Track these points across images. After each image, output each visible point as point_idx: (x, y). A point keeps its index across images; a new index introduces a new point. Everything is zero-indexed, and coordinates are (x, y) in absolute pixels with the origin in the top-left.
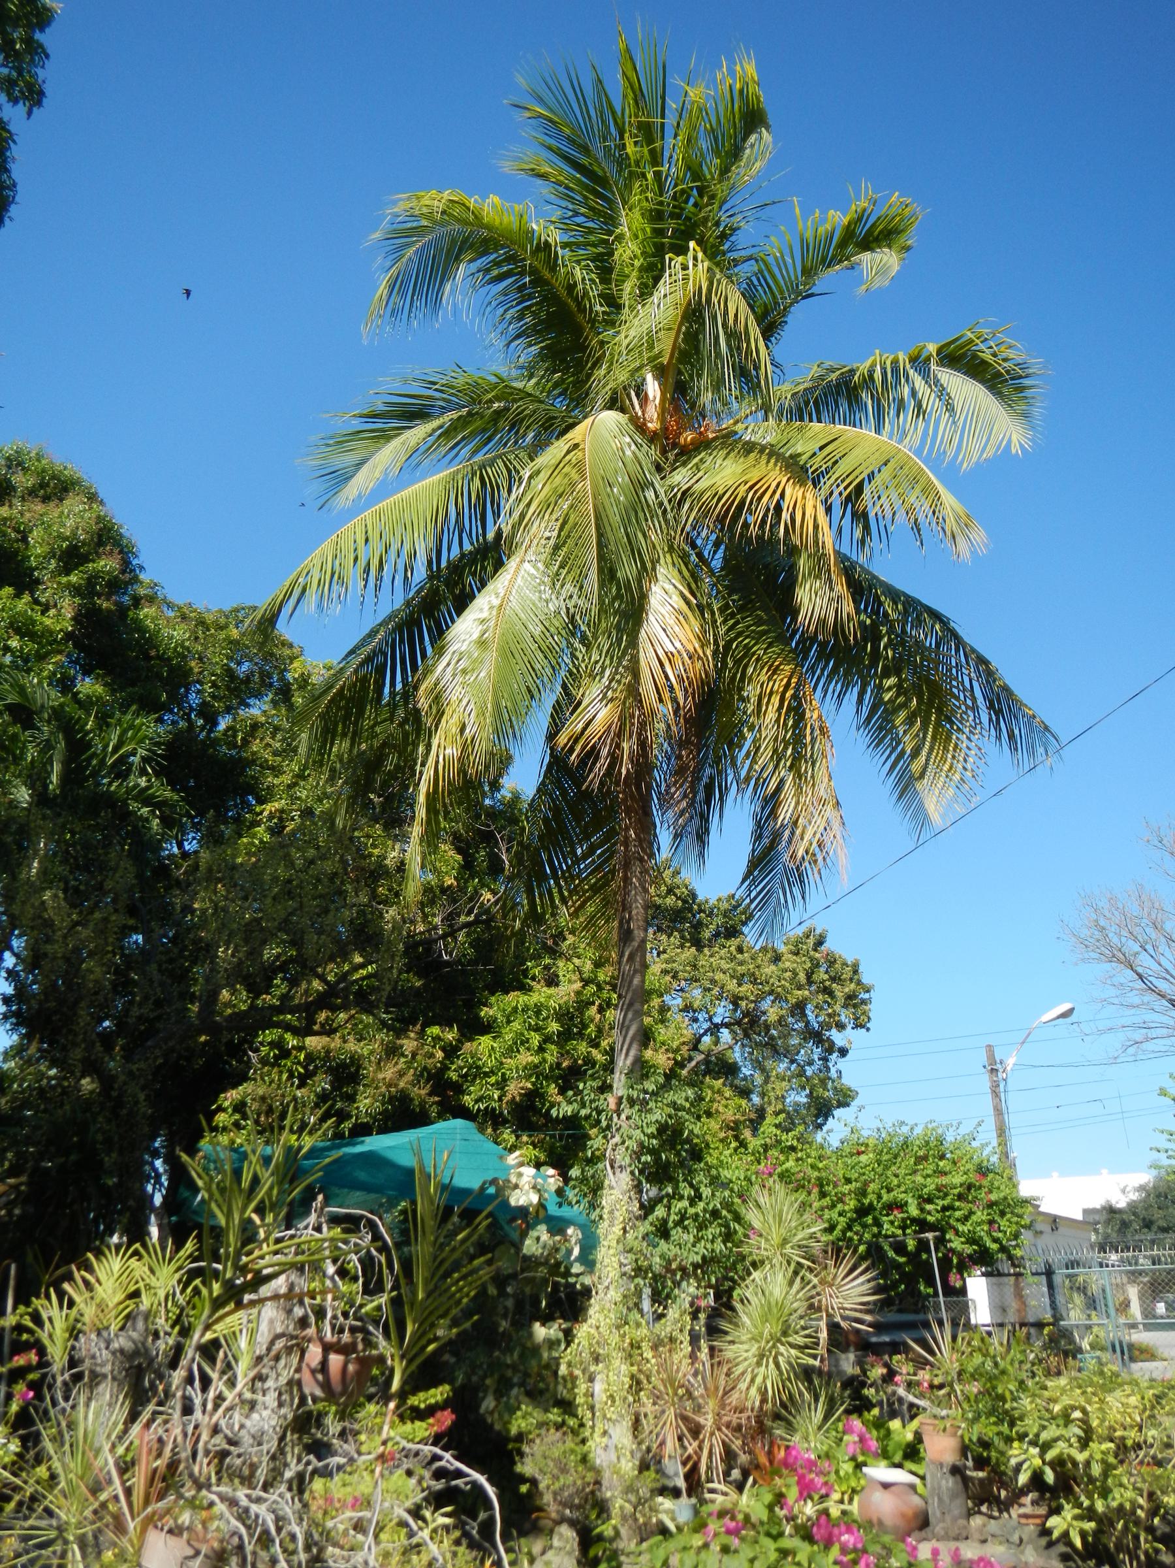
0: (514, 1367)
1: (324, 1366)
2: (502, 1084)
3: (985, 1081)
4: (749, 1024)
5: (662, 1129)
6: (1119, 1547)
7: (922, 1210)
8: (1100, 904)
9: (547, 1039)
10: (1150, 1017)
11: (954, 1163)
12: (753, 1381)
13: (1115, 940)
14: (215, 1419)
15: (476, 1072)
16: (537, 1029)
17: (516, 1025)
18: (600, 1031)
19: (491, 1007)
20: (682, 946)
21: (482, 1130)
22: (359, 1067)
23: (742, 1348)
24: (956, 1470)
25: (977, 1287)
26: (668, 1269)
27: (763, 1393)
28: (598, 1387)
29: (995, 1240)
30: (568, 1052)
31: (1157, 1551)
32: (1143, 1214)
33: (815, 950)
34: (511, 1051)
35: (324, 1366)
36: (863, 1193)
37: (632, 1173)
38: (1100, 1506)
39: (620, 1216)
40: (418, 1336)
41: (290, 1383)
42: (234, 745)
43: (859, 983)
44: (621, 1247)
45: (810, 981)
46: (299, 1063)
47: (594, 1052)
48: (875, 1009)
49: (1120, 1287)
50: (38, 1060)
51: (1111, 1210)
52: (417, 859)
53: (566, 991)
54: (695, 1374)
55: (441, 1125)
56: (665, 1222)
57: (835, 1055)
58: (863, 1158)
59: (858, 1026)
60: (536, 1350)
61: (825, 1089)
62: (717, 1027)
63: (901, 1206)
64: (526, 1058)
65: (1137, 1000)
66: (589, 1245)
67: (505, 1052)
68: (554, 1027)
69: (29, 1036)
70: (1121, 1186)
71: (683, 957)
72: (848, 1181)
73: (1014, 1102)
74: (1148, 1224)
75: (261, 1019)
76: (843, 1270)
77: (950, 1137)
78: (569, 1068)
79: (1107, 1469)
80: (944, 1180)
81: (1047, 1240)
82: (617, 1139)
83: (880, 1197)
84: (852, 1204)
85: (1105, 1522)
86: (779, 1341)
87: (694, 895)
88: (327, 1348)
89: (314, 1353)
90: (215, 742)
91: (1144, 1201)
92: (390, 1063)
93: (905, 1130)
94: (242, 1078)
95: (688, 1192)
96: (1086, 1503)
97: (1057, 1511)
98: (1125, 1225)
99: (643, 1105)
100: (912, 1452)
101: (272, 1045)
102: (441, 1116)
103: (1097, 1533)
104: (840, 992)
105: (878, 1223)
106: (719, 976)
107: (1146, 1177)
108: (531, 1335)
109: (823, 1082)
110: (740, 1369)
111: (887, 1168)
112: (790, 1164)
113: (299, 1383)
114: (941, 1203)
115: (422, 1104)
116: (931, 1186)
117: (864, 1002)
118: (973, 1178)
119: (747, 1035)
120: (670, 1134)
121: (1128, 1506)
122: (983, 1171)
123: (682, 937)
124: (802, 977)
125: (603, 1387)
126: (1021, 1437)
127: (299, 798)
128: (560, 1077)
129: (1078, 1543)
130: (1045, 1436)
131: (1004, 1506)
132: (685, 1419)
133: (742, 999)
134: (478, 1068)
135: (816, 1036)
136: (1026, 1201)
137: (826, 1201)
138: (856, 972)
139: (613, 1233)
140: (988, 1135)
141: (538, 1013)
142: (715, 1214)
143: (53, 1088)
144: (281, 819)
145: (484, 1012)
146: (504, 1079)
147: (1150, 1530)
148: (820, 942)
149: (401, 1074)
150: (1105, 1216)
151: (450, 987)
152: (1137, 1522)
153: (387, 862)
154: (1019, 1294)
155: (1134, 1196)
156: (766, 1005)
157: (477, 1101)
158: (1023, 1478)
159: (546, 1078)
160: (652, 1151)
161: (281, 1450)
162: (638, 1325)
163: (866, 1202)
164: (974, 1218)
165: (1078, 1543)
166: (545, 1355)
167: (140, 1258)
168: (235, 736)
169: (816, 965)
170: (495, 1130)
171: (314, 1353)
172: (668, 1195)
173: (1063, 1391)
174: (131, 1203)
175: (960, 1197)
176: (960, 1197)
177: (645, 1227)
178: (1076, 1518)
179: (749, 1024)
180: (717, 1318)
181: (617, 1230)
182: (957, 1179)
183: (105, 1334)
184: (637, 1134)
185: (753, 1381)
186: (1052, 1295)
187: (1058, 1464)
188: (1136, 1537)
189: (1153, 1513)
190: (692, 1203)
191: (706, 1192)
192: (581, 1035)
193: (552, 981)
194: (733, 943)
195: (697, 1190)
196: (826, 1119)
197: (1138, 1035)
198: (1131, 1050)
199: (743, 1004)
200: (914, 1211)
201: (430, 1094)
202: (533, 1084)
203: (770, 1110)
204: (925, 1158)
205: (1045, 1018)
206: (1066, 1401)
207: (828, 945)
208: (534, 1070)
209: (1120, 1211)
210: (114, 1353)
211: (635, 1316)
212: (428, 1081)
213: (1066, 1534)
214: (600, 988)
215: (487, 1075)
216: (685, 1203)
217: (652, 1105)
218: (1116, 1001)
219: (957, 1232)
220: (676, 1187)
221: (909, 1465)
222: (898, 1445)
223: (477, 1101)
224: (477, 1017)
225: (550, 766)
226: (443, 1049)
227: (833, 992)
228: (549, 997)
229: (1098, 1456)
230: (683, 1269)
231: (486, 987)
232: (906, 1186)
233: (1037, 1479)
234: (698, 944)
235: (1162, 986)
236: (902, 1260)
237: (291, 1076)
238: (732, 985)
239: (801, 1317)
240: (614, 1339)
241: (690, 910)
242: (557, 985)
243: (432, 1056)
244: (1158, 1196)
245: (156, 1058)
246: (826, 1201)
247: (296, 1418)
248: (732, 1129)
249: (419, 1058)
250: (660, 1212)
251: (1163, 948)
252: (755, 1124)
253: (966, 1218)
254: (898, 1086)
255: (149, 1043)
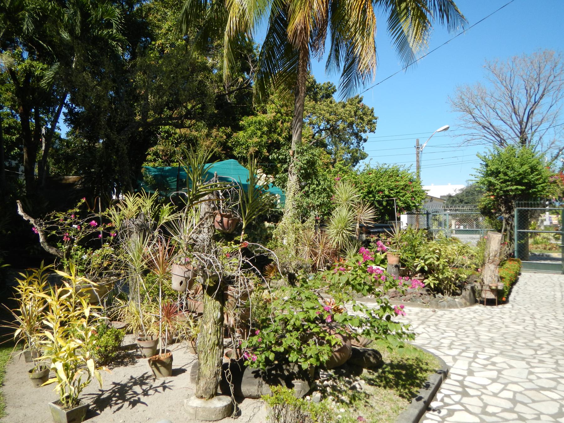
0: (258, 235)
1: (222, 221)
2: (248, 148)
3: (414, 151)
4: (333, 130)
5: (308, 162)
6: (445, 288)
7: (389, 193)
8: (464, 90)
9: (263, 133)
10: (475, 131)
11: (402, 178)
12: (334, 240)
13: (467, 104)
14: (190, 235)
15: (238, 144)
16: (260, 129)
17: (252, 128)
18: (282, 130)
19: (243, 121)
20: (310, 101)
21: (240, 163)
22: (197, 141)
23: (331, 231)
24: (396, 266)
25: (404, 218)
26: (308, 207)
27: (338, 243)
28: (285, 242)
29: (413, 203)
30: (270, 138)
31: (456, 289)
32: (460, 198)
33: (359, 104)
34: (251, 137)
35: (222, 221)
36: (370, 187)
37: (298, 176)
38: (441, 277)
39: (293, 190)
40: (250, 214)
41: (211, 226)
42: (141, 17)
43: (373, 116)
44: (293, 199)
45: (355, 115)
46: (175, 139)
47: (280, 138)
48: (379, 125)
49: (450, 220)
50: (79, 136)
51: (450, 196)
52: (221, 63)
53: (270, 116)
54: (316, 238)
55: (226, 161)
56: (308, 192)
57: (362, 141)
58: (371, 176)
59: (371, 131)
60: (265, 230)
61: (357, 153)
62: (321, 130)
63: (382, 191)
64: (256, 139)
65: (471, 126)
66: (283, 198)
67: (249, 136)
68: (265, 129)
69: (75, 128)
70: (454, 188)
71: (310, 104)
72: (365, 183)
73: (423, 157)
74: (461, 201)
75: (159, 122)
76: (365, 208)
77: (401, 169)
78: (270, 143)
79: (444, 267)
80: (398, 183)
81: (428, 204)
82: (293, 165)
83: (375, 188)
84: (366, 190)
85: (441, 281)
86: (344, 229)
87: (315, 82)
88: (222, 216)
89: (218, 218)
90: (133, 15)
91: (462, 193)
92: (208, 138)
93: (386, 166)
94: (155, 143)
95: (316, 182)
96: (437, 276)
97: (427, 278)
98: (454, 201)
99: (302, 153)
100: (383, 262)
101: (165, 132)
102: (226, 158)
103: (438, 284)
104: (366, 119)
105: (374, 197)
106: (323, 112)
107: (463, 186)
108: (264, 225)
109: (357, 151)
110: (330, 237)
111: (379, 179)
112: (346, 176)
113: (214, 226)
114: (396, 191)
115: (220, 153)
116: (393, 185)
117: (374, 123)
118: (408, 183)
119: (331, 134)
120: (311, 163)
121: (449, 277)
122: (411, 181)
123: (310, 97)
124: (353, 113)
125: (288, 240)
126: (418, 257)
127: (169, 39)
128: (268, 146)
129: (432, 286)
130: (426, 257)
131: (410, 277)
132: (312, 251)
133: (330, 120)
134: (239, 142)
135: (356, 135)
136: (423, 191)
137: (358, 189)
138: (372, 112)
139: (289, 196)
140: (414, 170)
141: (260, 123)
142: (325, 190)
143: (86, 146)
144: (162, 47)
145: (241, 123)
146: (248, 146)
147: (455, 284)
148: (360, 101)
149: (212, 143)
150: (448, 198)
151: (229, 112)
152: (451, 281)
153: (208, 65)
154: (417, 220)
155: (458, 192)
156: (339, 123)
157: (238, 154)
158: (418, 269)
159: (262, 146)
160: (304, 169)
161: (210, 244)
162: (298, 223)
163: (371, 189)
164: (406, 196)
165: (432, 286)
166: (269, 232)
167: (140, 197)
168: (142, 13)
169: (358, 109)
170: (244, 163)
171: (218, 218)
172: (309, 183)
173: (434, 244)
174: (125, 183)
175: (402, 189)
176: (402, 189)
177: (301, 193)
178: (433, 280)
179: (333, 130)
180: (322, 224)
181: (292, 194)
182: (402, 183)
183: (132, 219)
184: (300, 163)
185: (334, 240)
186: (428, 221)
187: (430, 265)
188: (450, 286)
189: (457, 279)
190: (317, 185)
191: (322, 183)
192: (275, 132)
193: (265, 112)
194: (329, 100)
195: (319, 182)
196: (356, 164)
197: (469, 138)
198: (466, 143)
199: (331, 122)
200: (387, 193)
201: (222, 150)
202: (258, 149)
203: (338, 159)
204: (392, 176)
205: (438, 130)
206: (434, 247)
207: (363, 102)
208: (259, 144)
209: (452, 197)
210: (135, 225)
211: (297, 220)
212: (221, 146)
213: (429, 284)
214: (282, 115)
215: (242, 145)
216: (315, 186)
217: (305, 153)
218: (463, 126)
219: (400, 200)
220: (312, 181)
221: (382, 265)
222: (379, 260)
223: (238, 154)
224: (238, 124)
225: (270, 27)
226: (226, 135)
227: (363, 119)
228: (264, 118)
229: (442, 263)
230: (313, 207)
231: (240, 113)
232: (385, 185)
233: (423, 268)
234: (316, 100)
235: (481, 121)
236: (381, 208)
237: (173, 143)
238: (327, 115)
239: (352, 222)
240: (290, 227)
241: (313, 87)
242: (266, 113)
243: (222, 137)
244: (467, 192)
245: (129, 135)
246: (358, 189)
247: (214, 236)
248: (326, 165)
249: (217, 138)
250: (306, 189)
251: (483, 107)
252: (333, 164)
253: (404, 196)
254: (382, 152)
255: (126, 129)
